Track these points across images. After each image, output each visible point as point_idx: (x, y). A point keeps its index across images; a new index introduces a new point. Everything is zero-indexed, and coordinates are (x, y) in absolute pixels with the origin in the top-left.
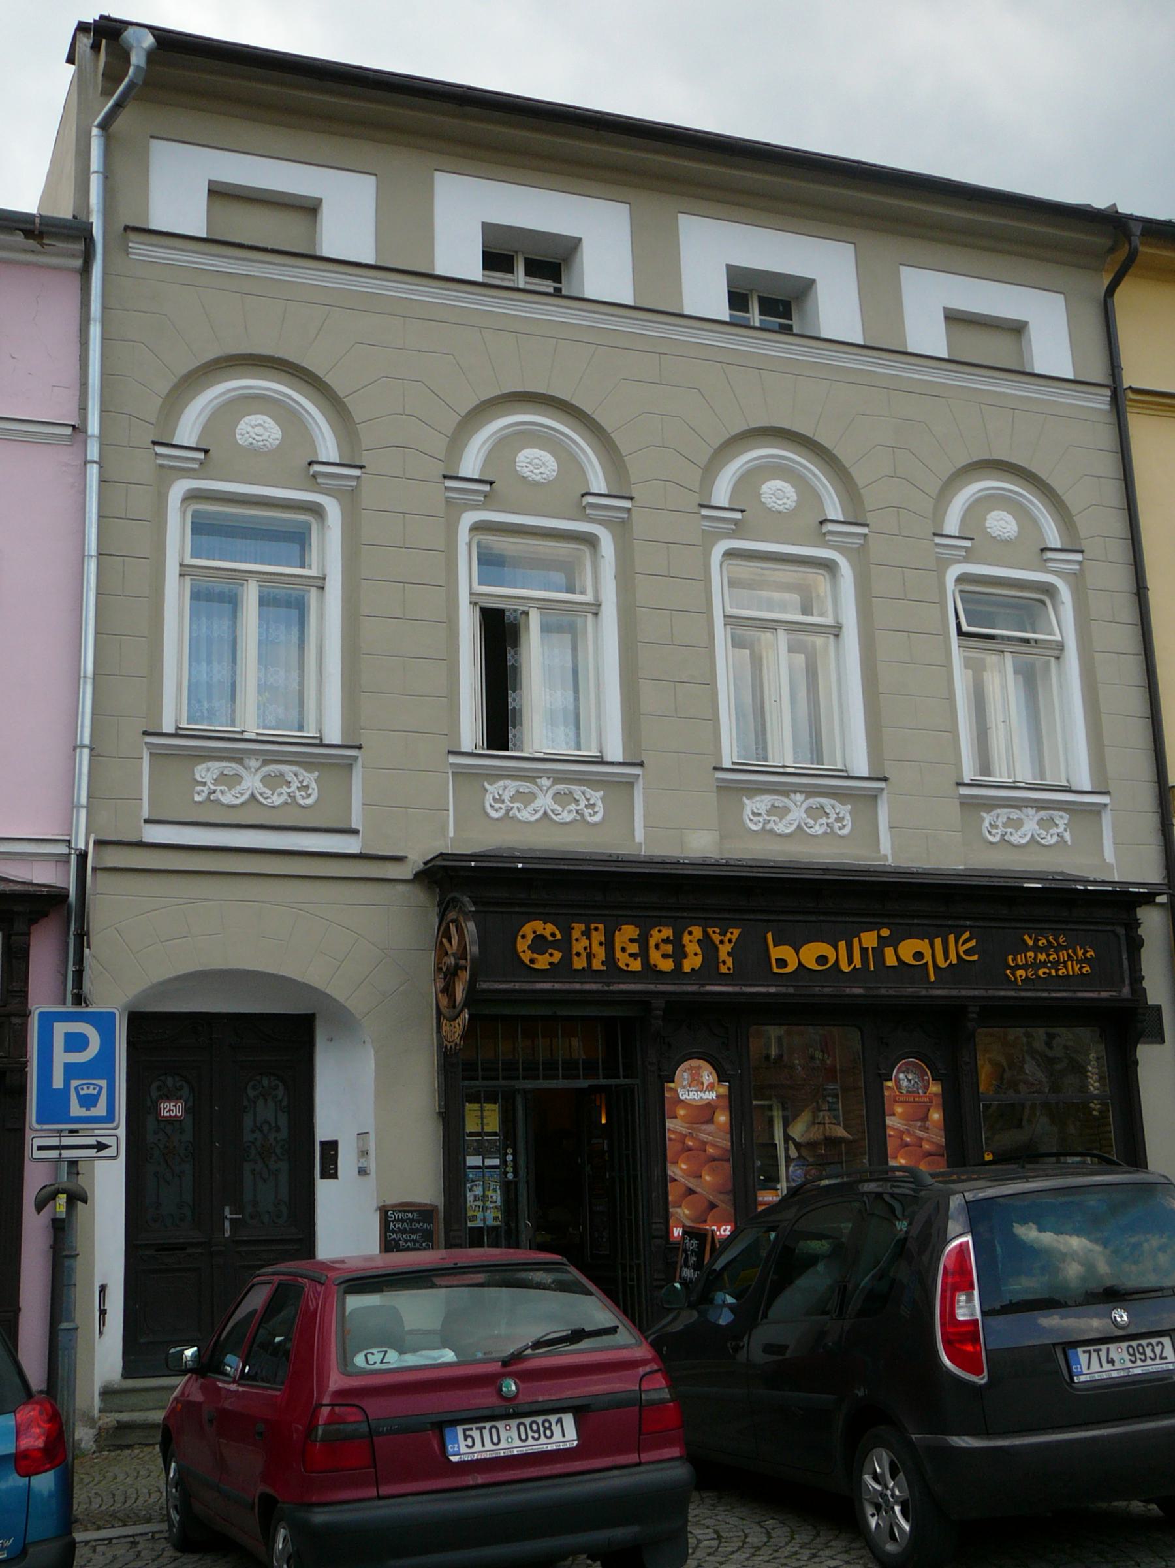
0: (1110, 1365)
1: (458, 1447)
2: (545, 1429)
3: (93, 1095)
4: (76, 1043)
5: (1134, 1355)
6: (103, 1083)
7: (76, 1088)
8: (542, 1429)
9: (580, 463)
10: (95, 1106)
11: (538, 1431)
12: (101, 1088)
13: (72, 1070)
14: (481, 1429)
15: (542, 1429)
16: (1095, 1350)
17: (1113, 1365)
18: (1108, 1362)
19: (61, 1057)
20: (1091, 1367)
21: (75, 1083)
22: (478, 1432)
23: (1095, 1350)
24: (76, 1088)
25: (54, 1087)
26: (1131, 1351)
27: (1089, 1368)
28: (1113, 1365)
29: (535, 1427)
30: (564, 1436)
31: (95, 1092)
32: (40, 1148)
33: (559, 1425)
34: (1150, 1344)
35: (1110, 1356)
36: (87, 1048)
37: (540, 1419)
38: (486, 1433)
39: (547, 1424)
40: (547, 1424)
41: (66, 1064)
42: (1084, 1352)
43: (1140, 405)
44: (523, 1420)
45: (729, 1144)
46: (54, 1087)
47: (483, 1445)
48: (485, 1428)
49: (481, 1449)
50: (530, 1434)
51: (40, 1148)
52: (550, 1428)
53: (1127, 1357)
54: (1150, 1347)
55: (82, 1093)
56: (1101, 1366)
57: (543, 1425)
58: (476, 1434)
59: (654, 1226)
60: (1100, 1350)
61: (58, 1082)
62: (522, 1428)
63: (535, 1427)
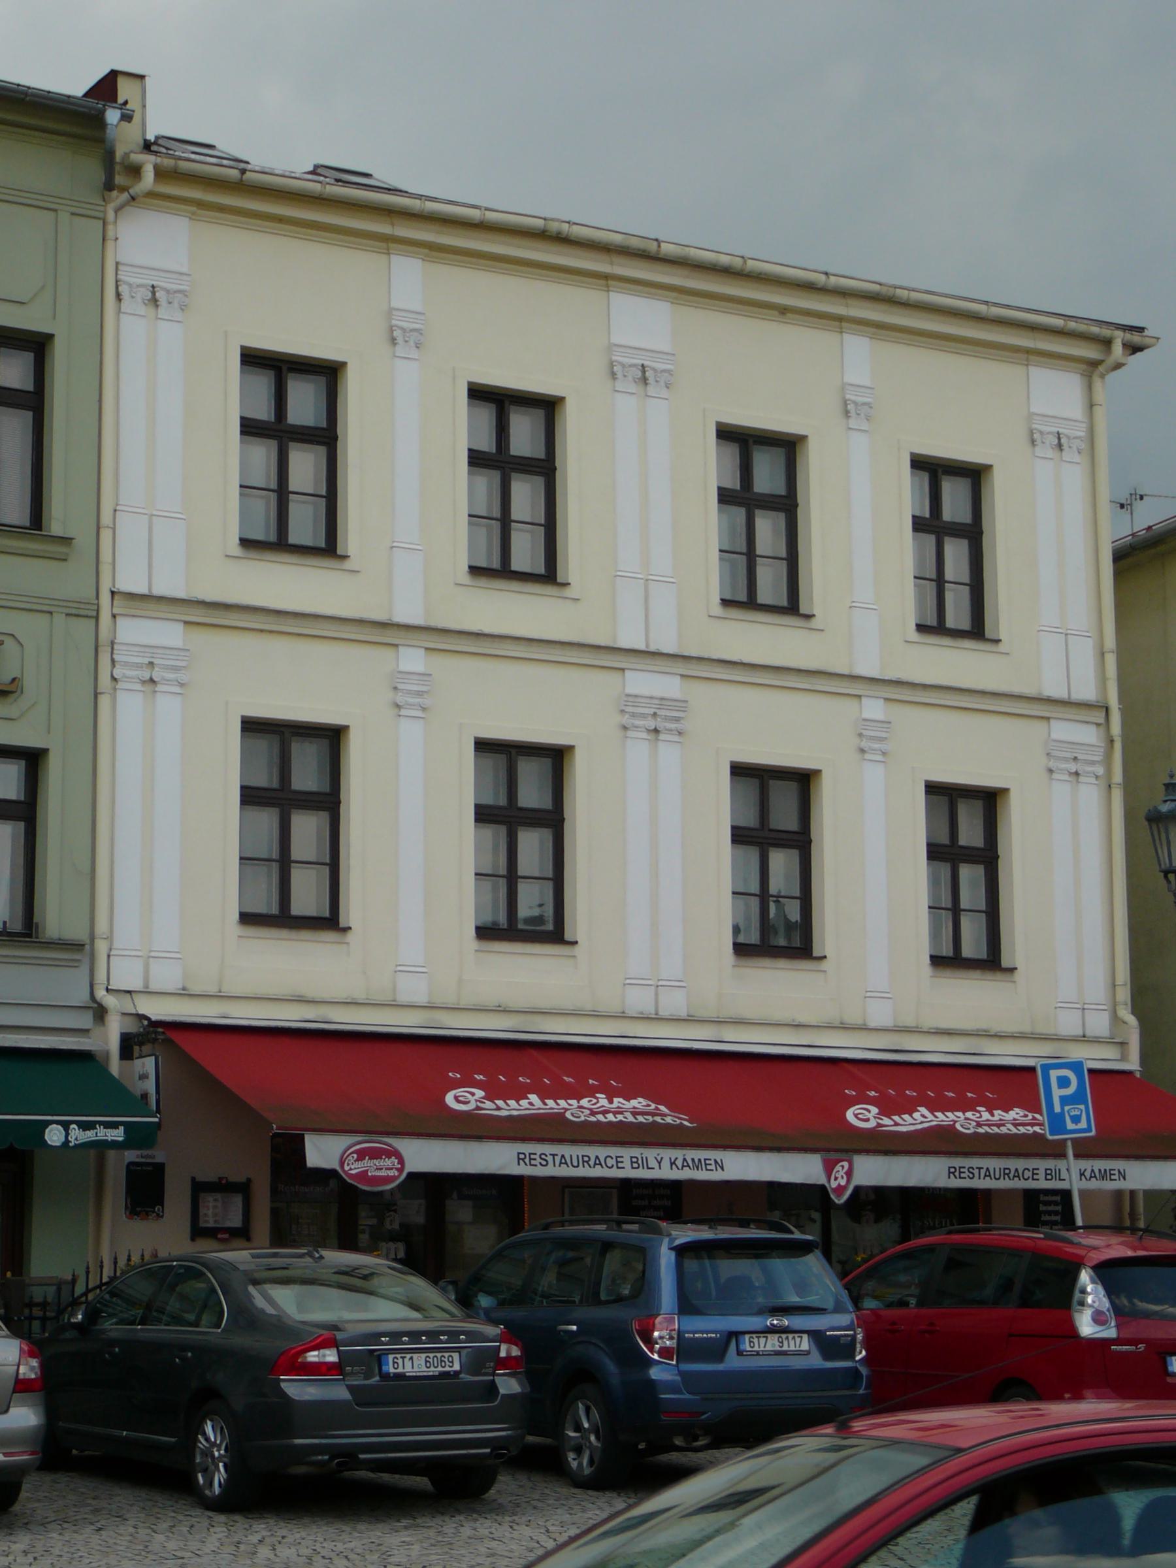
3: (1077, 1115)
4: (1064, 1082)
5: (442, 1361)
6: (1082, 1107)
7: (1068, 1112)
10: (1080, 1122)
12: (1082, 1111)
13: (1064, 1100)
14: (403, 1358)
16: (401, 1357)
19: (1057, 1093)
20: (406, 1367)
21: (1067, 1108)
24: (1068, 1112)
25: (1056, 1111)
26: (780, 1340)
27: (765, 1347)
31: (1079, 1113)
34: (436, 1356)
38: (406, 1360)
41: (1060, 1097)
44: (437, 1354)
45: (211, 1224)
46: (1056, 1111)
50: (431, 1360)
53: (777, 1343)
55: (1072, 1114)
56: (413, 1368)
59: (1059, 1208)
60: (405, 1357)
61: (1057, 1109)
62: (435, 1359)
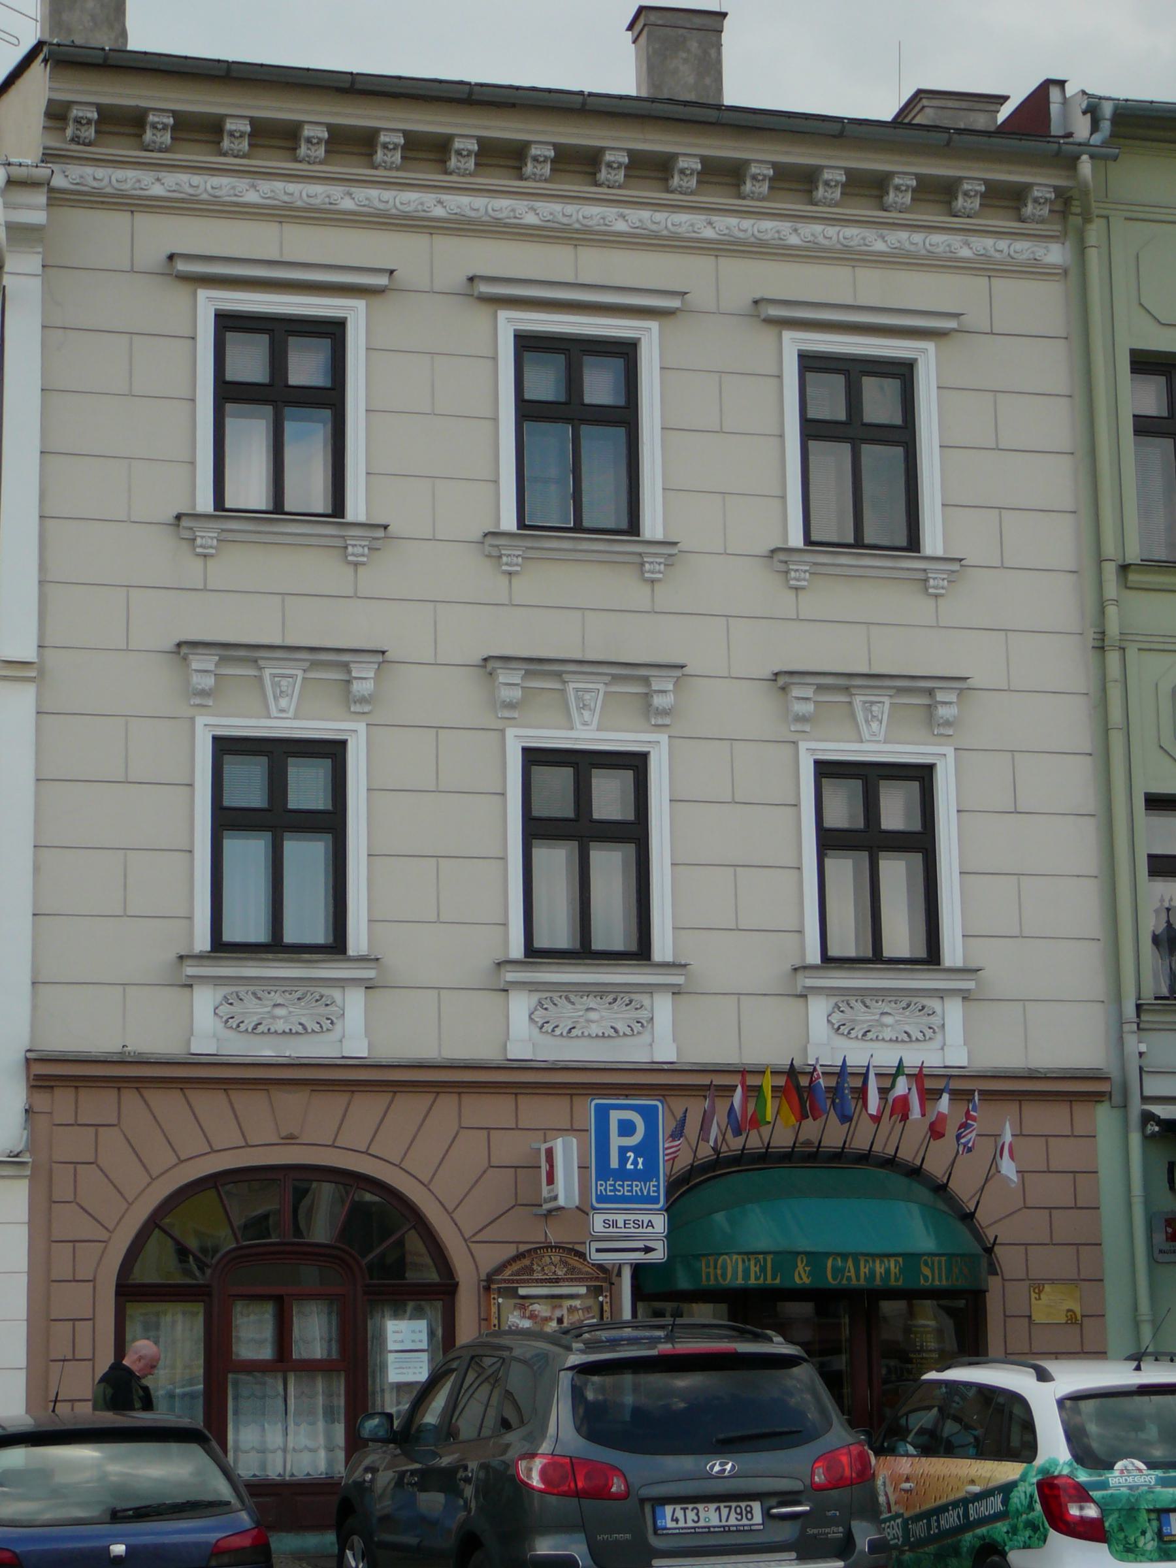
0: (675, 1523)
1: (666, 1523)
2: (747, 1512)
8: (744, 1513)
9: (406, 1201)
11: (741, 1514)
15: (744, 1513)
17: (677, 1523)
18: (672, 1520)
22: (682, 1511)
23: (681, 1509)
27: (727, 1521)
28: (677, 1523)
29: (738, 1510)
30: (721, 1521)
32: (598, 1250)
33: (718, 1512)
35: (676, 1515)
36: (635, 1126)
37: (743, 1505)
38: (688, 1512)
39: (748, 1509)
40: (748, 1509)
42: (725, 1507)
43: (911, 106)
47: (686, 1522)
48: (687, 1508)
49: (684, 1525)
51: (598, 1250)
52: (751, 1512)
54: (695, 1511)
57: (746, 1509)
58: (725, 1512)
63: (738, 1510)
